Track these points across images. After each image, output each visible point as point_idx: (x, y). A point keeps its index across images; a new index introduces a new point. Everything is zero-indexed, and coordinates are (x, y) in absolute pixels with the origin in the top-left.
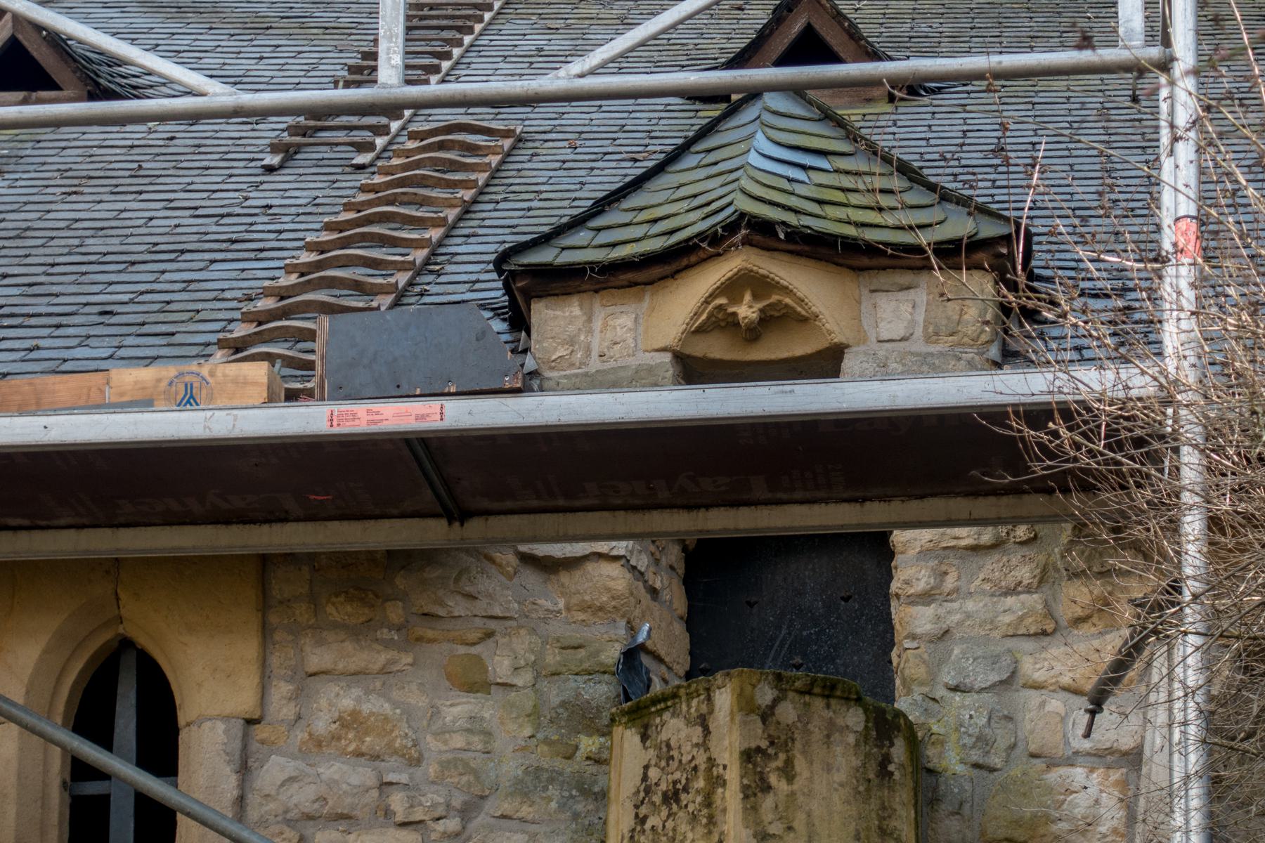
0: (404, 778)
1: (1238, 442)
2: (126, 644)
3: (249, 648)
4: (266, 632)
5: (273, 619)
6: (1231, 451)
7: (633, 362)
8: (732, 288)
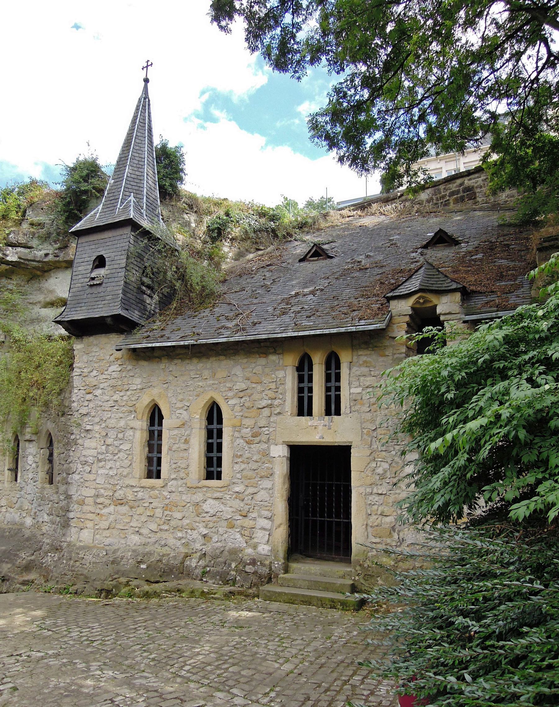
8: (419, 298)
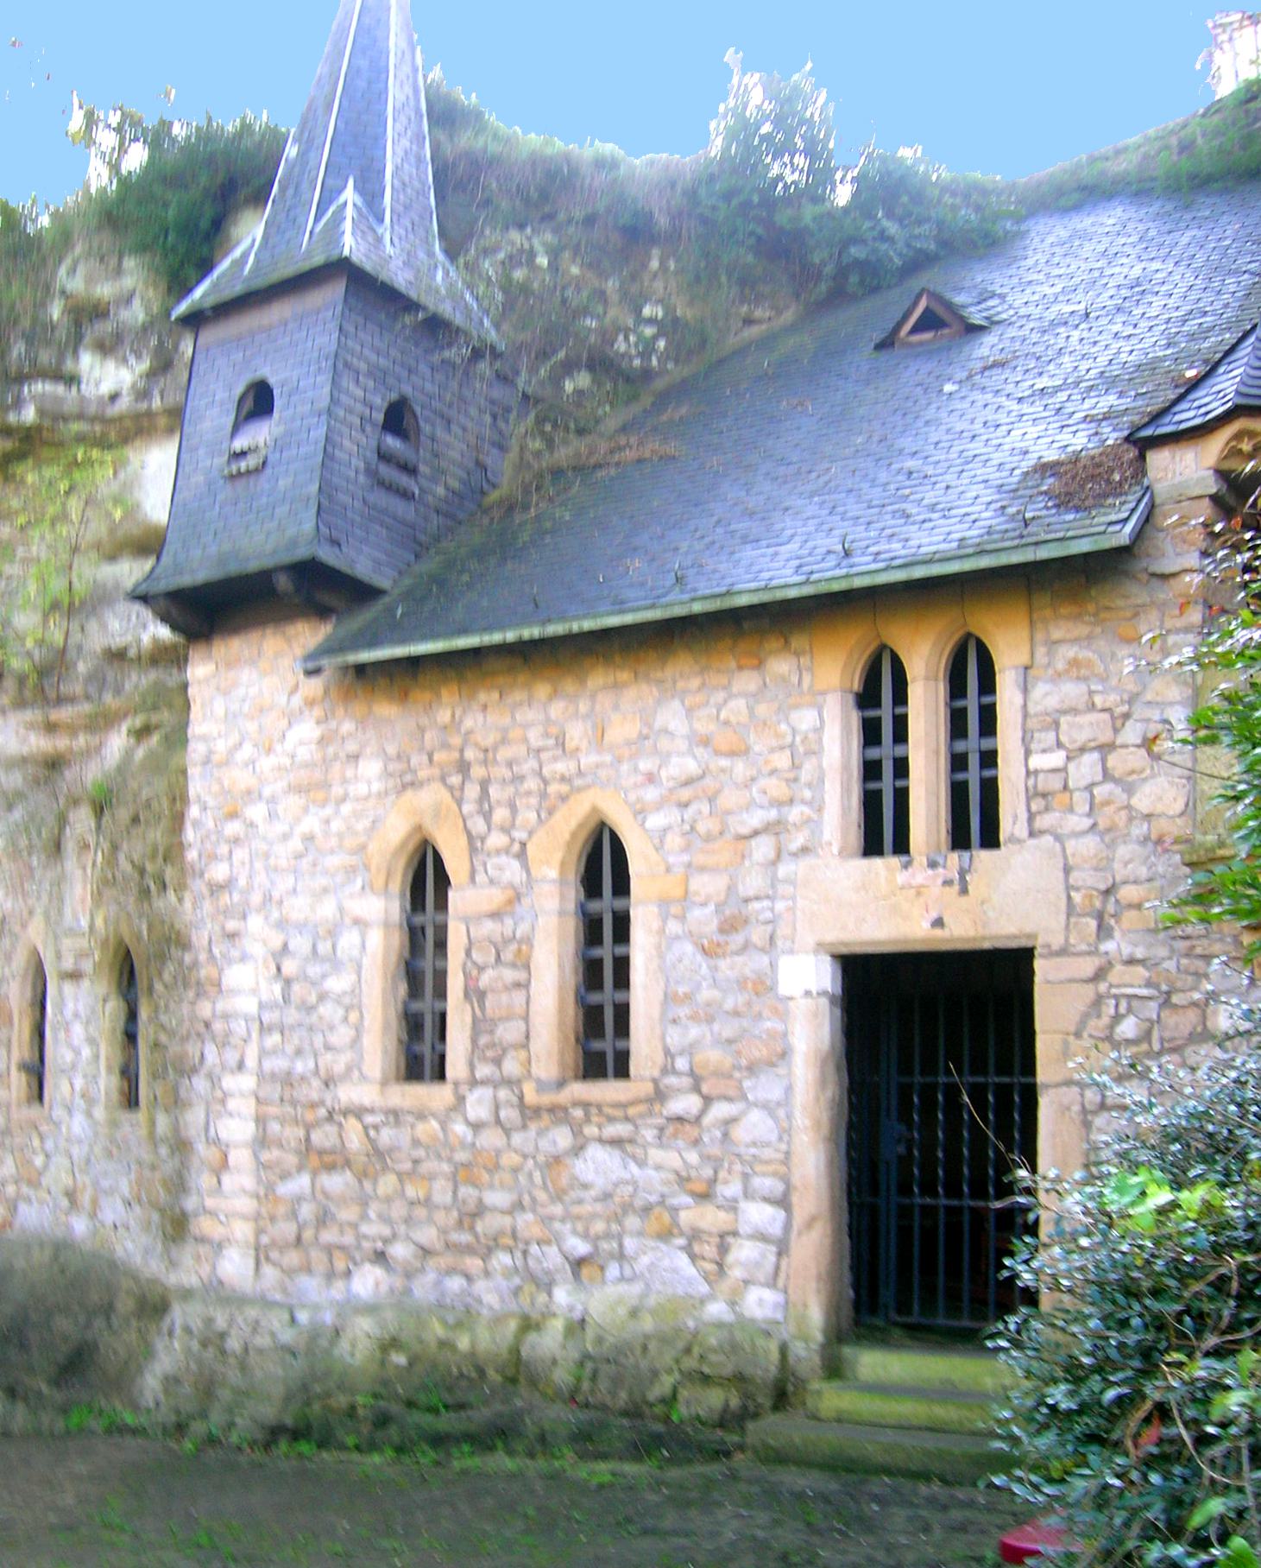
0: (1100, 688)
1: (463, 1174)
2: (969, 635)
3: (1025, 633)
4: (1032, 624)
5: (1035, 616)
6: (632, 338)
7: (1195, 476)
8: (1238, 436)
